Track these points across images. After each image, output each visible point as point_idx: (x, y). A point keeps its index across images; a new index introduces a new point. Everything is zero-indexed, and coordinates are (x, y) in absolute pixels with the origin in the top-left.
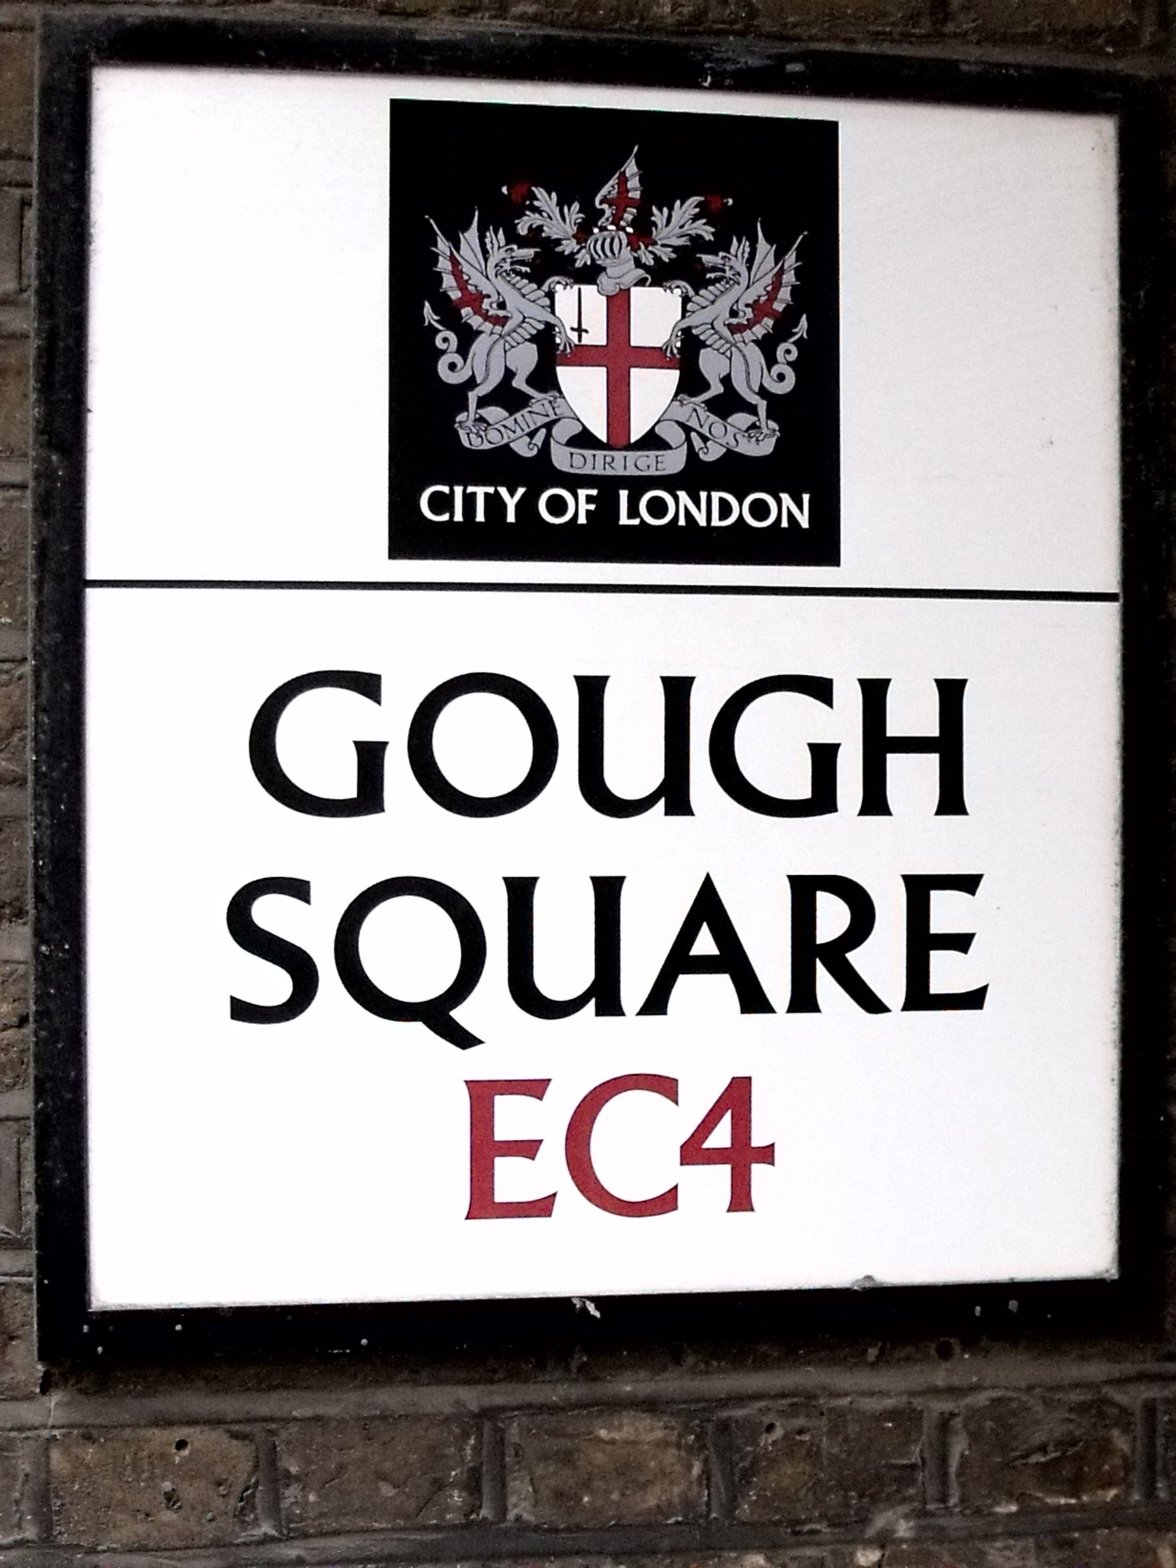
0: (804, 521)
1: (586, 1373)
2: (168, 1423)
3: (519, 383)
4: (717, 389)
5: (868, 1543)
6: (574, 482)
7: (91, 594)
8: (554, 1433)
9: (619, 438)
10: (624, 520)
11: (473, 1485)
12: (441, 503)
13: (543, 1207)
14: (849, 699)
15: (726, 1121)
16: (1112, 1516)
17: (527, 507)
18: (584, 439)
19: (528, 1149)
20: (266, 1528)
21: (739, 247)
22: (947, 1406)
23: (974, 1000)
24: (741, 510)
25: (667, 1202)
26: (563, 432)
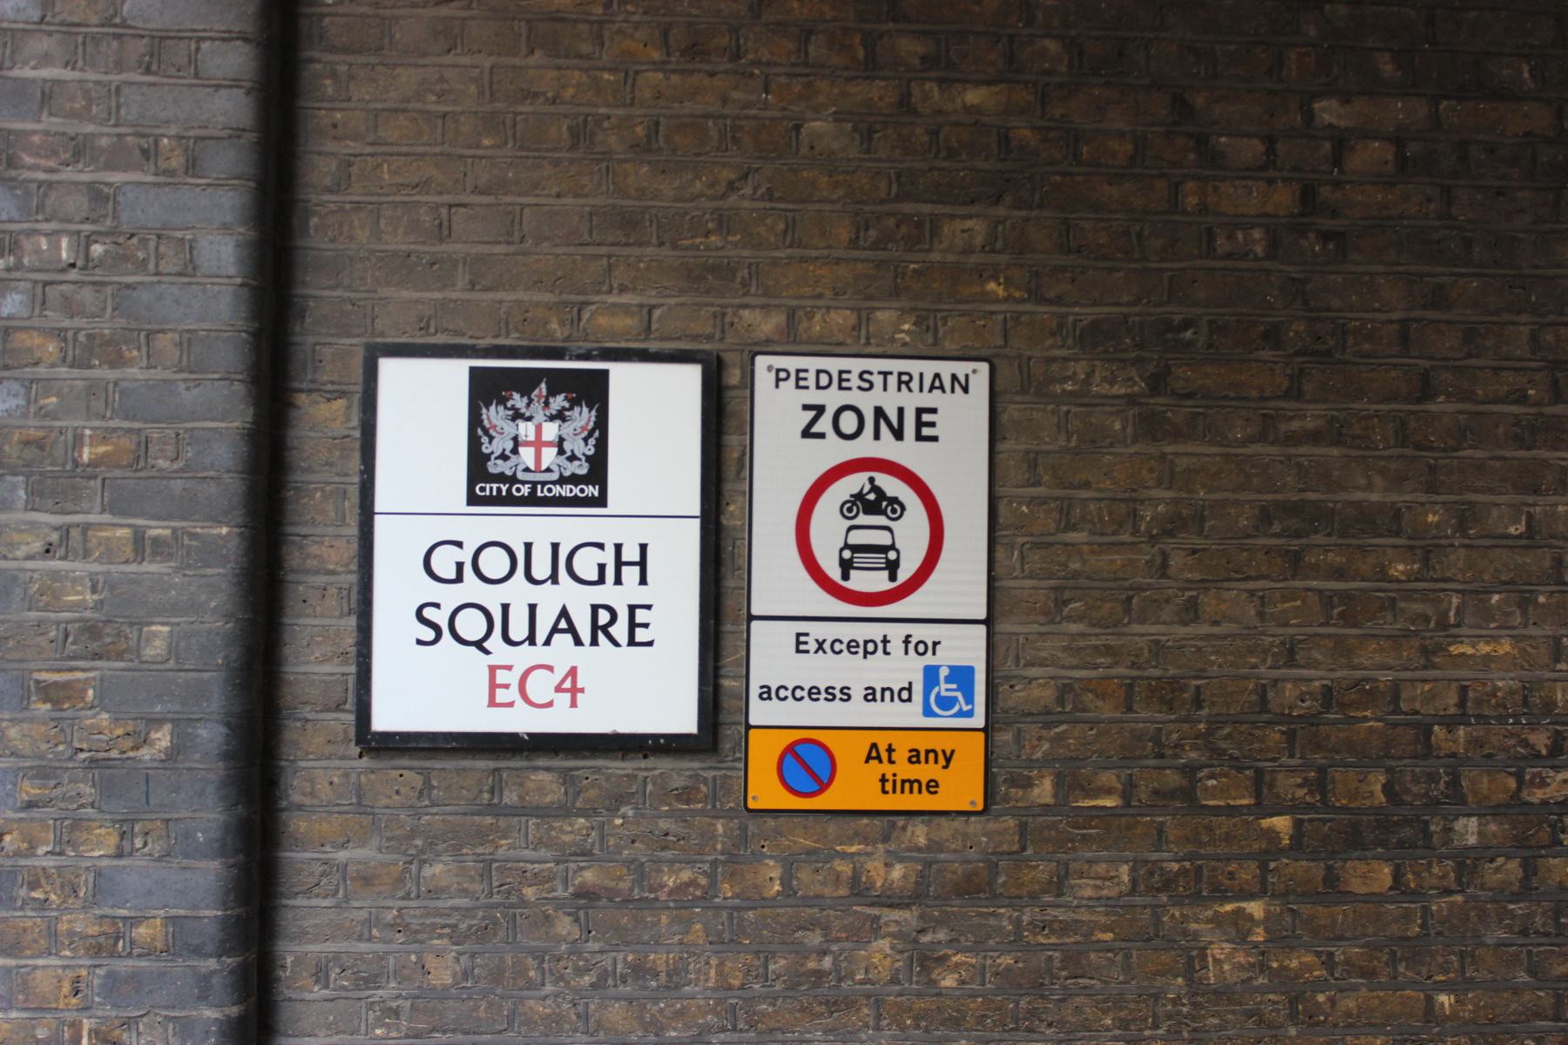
0: (596, 494)
1: (528, 759)
2: (397, 769)
3: (507, 453)
4: (569, 454)
5: (618, 817)
6: (524, 483)
7: (377, 517)
8: (518, 777)
9: (538, 470)
10: (539, 494)
11: (492, 791)
12: (483, 489)
13: (511, 705)
14: (610, 550)
15: (569, 679)
16: (702, 812)
17: (509, 490)
18: (527, 470)
19: (506, 686)
20: (427, 803)
21: (577, 409)
22: (645, 774)
23: (650, 644)
24: (576, 491)
25: (550, 704)
26: (521, 467)
